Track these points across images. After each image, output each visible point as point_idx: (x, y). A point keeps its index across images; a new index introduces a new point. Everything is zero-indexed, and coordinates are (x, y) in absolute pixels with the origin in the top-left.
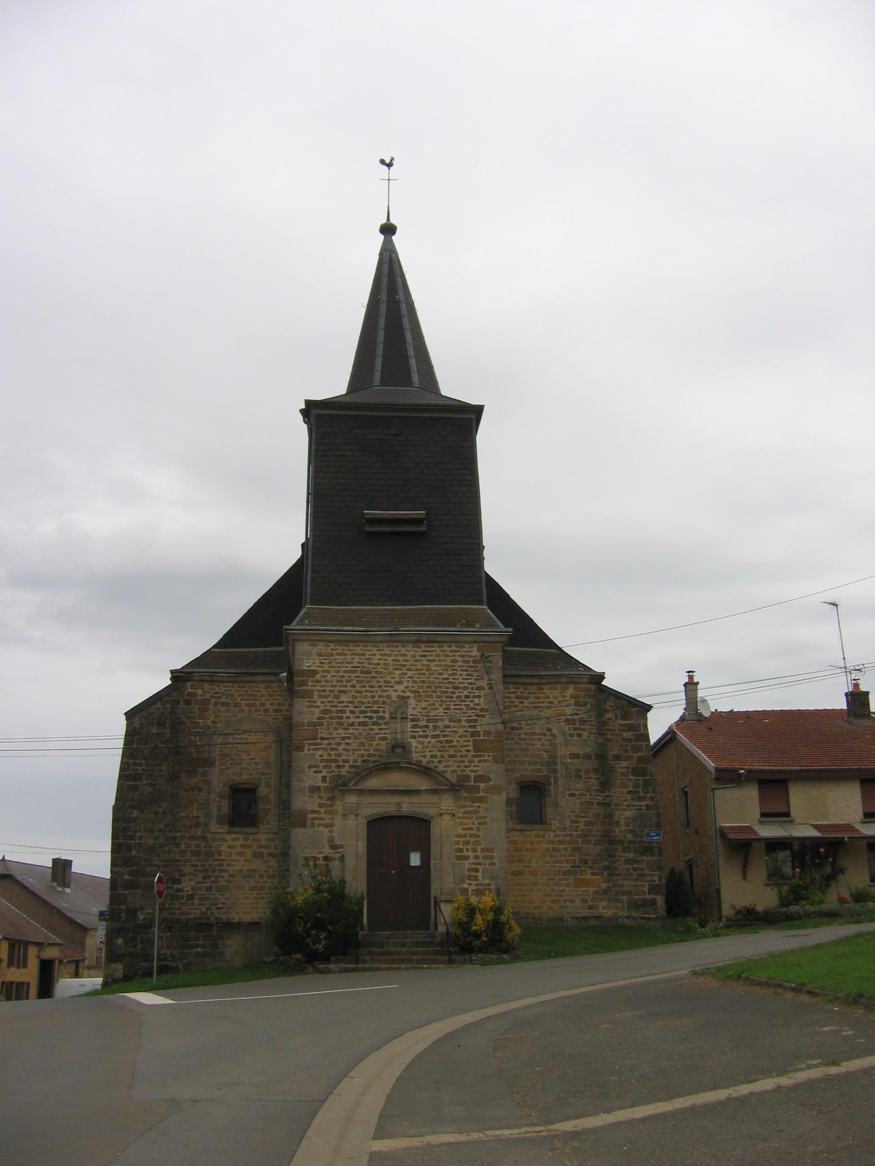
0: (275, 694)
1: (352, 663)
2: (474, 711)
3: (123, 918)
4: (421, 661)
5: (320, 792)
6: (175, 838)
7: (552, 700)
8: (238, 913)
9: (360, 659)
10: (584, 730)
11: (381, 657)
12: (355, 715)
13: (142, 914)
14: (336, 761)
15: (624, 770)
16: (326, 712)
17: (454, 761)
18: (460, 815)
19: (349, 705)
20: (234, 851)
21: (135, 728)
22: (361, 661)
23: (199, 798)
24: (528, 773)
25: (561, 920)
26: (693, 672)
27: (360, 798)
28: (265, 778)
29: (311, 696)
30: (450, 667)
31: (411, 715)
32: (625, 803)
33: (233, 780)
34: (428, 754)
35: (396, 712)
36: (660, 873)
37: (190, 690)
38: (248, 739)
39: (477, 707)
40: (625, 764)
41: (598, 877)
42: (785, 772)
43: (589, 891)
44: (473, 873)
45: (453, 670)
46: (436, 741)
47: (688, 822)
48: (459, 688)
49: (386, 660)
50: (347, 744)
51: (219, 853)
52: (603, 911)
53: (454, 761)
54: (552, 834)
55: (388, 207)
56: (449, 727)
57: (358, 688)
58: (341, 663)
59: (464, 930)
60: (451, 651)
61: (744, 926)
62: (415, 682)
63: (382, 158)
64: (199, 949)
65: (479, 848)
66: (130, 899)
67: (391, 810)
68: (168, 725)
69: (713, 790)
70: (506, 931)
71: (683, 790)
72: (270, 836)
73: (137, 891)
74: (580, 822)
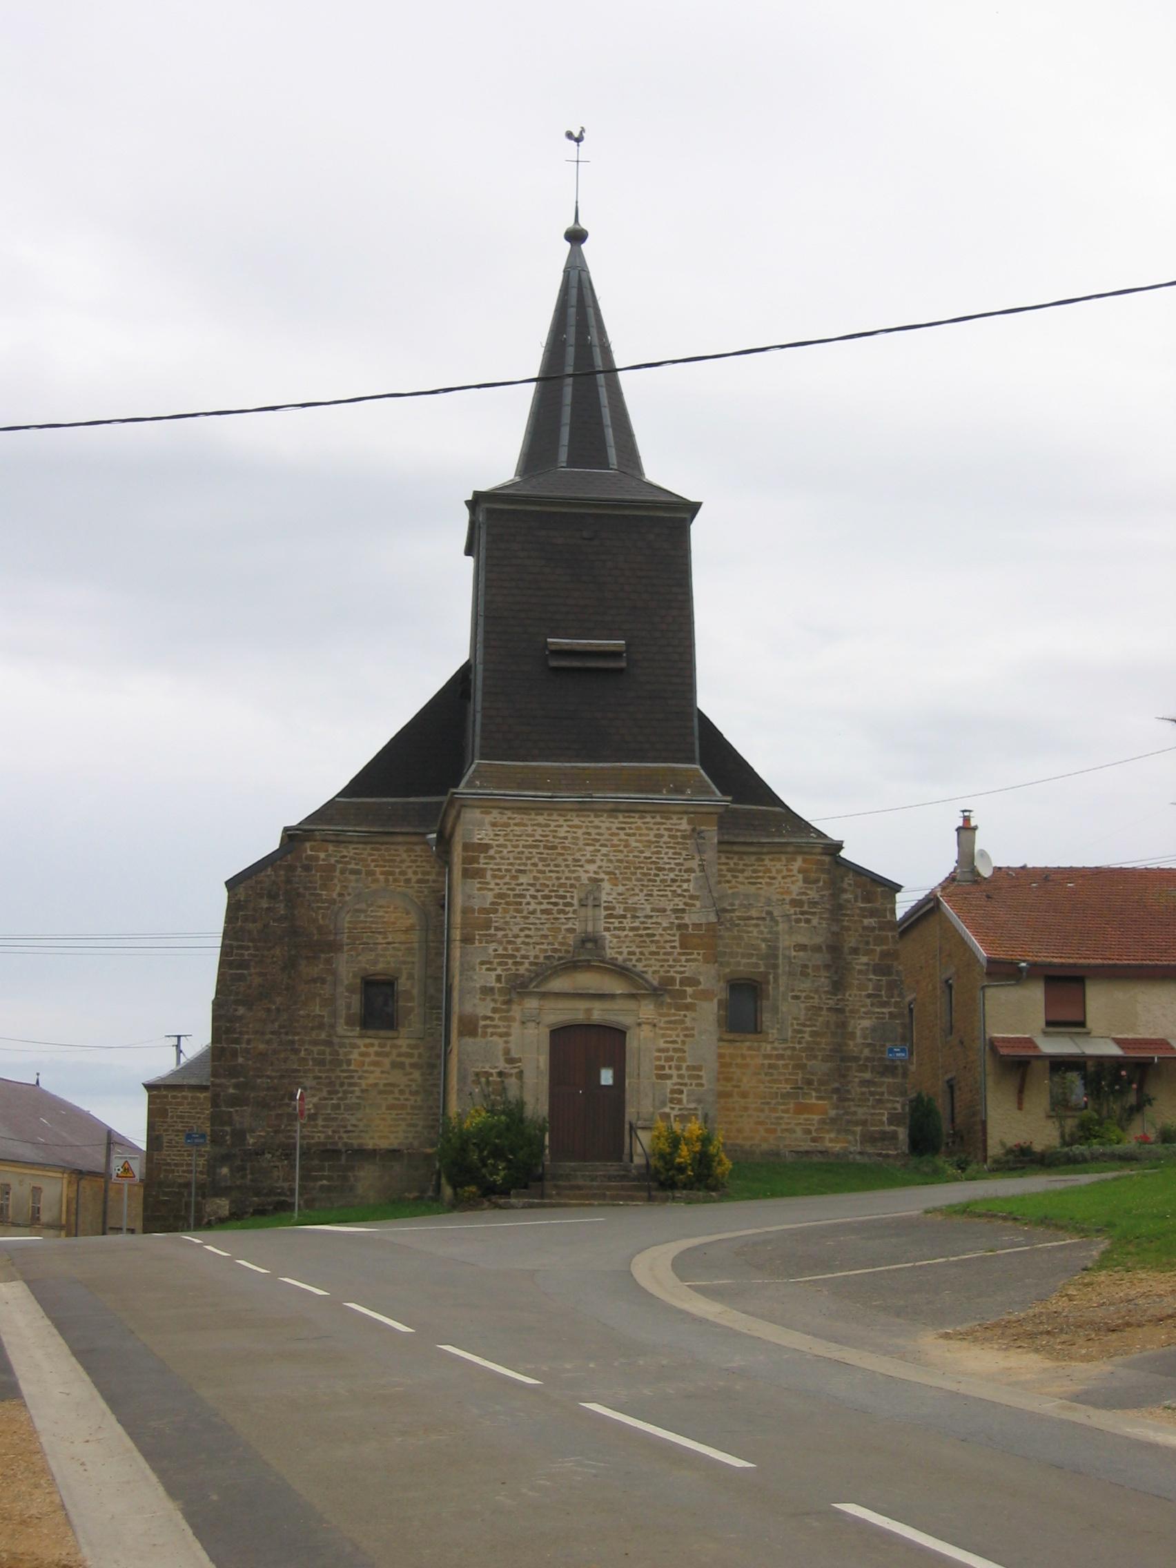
0: (420, 859)
1: (533, 836)
2: (681, 898)
3: (228, 1142)
4: (618, 834)
5: (494, 994)
6: (293, 1042)
7: (774, 874)
8: (372, 1138)
9: (543, 831)
10: (813, 914)
11: (569, 829)
12: (536, 901)
13: (251, 1137)
14: (513, 956)
15: (864, 968)
16: (500, 896)
17: (656, 959)
18: (662, 1025)
19: (529, 887)
20: (367, 1060)
21: (240, 901)
22: (544, 833)
23: (322, 992)
24: (742, 968)
25: (777, 1154)
26: (970, 811)
27: (542, 1002)
28: (406, 969)
29: (483, 876)
30: (653, 842)
31: (605, 902)
32: (863, 1010)
33: (365, 969)
34: (625, 950)
35: (587, 898)
36: (903, 1098)
37: (310, 853)
38: (384, 917)
39: (685, 893)
40: (864, 959)
41: (826, 1102)
42: (1082, 966)
43: (813, 1120)
44: (676, 1096)
45: (656, 847)
46: (635, 935)
47: (951, 1027)
48: (664, 869)
49: (575, 833)
50: (527, 936)
51: (349, 1062)
52: (830, 1145)
53: (656, 959)
54: (769, 1047)
55: (577, 202)
56: (651, 917)
57: (540, 867)
58: (520, 836)
59: (666, 1163)
60: (655, 824)
61: (1014, 1169)
62: (610, 861)
63: (572, 131)
64: (325, 1182)
65: (684, 1065)
66: (236, 1118)
67: (580, 1017)
68: (281, 898)
69: (983, 988)
70: (715, 1164)
71: (947, 981)
72: (413, 1042)
73: (245, 1108)
74: (804, 1032)
